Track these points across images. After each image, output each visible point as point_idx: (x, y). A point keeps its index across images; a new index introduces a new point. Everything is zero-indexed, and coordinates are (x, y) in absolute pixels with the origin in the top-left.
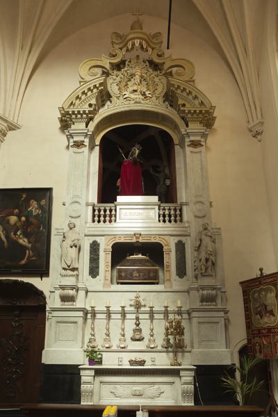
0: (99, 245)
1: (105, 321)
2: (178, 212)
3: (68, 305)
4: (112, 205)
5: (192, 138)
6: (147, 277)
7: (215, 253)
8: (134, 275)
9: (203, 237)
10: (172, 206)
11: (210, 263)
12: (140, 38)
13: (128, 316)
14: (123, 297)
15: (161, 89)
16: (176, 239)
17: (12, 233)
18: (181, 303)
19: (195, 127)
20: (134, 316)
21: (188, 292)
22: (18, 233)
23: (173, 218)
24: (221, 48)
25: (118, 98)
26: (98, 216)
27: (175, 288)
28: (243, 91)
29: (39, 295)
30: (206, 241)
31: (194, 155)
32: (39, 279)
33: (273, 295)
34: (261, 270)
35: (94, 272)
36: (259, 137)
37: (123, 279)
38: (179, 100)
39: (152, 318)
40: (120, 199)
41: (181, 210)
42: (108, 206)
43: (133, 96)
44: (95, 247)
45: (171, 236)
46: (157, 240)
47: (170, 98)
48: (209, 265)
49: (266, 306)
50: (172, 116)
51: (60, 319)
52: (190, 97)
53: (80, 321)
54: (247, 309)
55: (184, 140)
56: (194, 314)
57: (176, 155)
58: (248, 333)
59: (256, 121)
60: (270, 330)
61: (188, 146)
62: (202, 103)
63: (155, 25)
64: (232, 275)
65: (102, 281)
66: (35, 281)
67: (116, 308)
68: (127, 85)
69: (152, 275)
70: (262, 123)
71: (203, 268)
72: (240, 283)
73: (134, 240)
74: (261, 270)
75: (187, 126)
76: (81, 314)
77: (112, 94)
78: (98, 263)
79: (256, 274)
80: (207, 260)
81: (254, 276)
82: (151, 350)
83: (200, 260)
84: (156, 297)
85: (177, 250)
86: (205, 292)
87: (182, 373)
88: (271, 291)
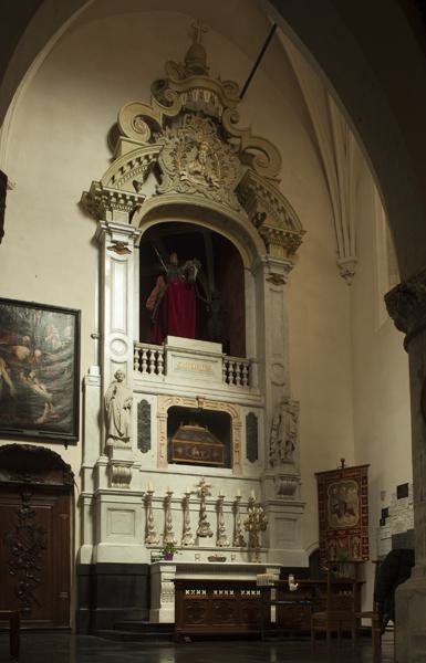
0: (149, 407)
1: (162, 512)
2: (160, 359)
3: (120, 487)
4: (161, 348)
5: (273, 270)
6: (208, 456)
7: (294, 436)
8: (194, 453)
9: (284, 413)
10: (239, 361)
11: (290, 447)
12: (211, 91)
13: (191, 507)
14: (184, 481)
15: (233, 179)
16: (248, 410)
17: (22, 374)
18: (242, 492)
19: (277, 253)
20: (198, 507)
21: (260, 481)
22: (32, 375)
23: (238, 378)
24: (312, 128)
25: (172, 177)
26: (144, 363)
27: (245, 474)
28: (335, 205)
29: (64, 469)
30: (287, 418)
31: (274, 295)
32: (63, 447)
33: (355, 491)
34: (343, 461)
35: (144, 444)
36: (349, 279)
37: (174, 456)
38: (259, 206)
39: (235, 512)
40: (172, 341)
41: (164, 356)
42: (154, 348)
43: (193, 180)
44: (144, 409)
45: (242, 405)
46: (219, 408)
47: (244, 194)
48: (285, 450)
49: (346, 504)
50: (243, 224)
51: (112, 506)
52: (275, 207)
53: (140, 510)
54: (322, 507)
55: (262, 269)
56: (272, 508)
57: (246, 285)
58: (321, 535)
59: (349, 259)
60: (347, 531)
61: (267, 280)
62: (289, 222)
63: (228, 63)
64: (310, 463)
65: (156, 457)
66: (57, 449)
67: (178, 495)
68: (184, 157)
69: (215, 454)
70: (355, 262)
71: (283, 452)
72: (316, 474)
73: (195, 405)
74: (343, 461)
75: (268, 252)
76: (139, 500)
77: (163, 168)
78: (149, 432)
79: (336, 465)
80: (287, 443)
81: (335, 468)
82: (220, 548)
83: (279, 442)
84: (224, 483)
85: (248, 425)
86: (285, 482)
87: (268, 570)
88: (353, 486)
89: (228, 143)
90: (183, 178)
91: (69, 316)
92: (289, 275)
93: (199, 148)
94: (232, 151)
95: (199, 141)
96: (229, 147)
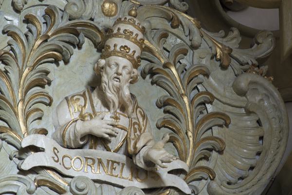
68: (42, 82)
89: (227, 26)
90: (31, 161)
91: (243, 109)
92: (58, 6)
93: (101, 48)
94: (247, 56)
95: (102, 22)
96: (233, 41)
